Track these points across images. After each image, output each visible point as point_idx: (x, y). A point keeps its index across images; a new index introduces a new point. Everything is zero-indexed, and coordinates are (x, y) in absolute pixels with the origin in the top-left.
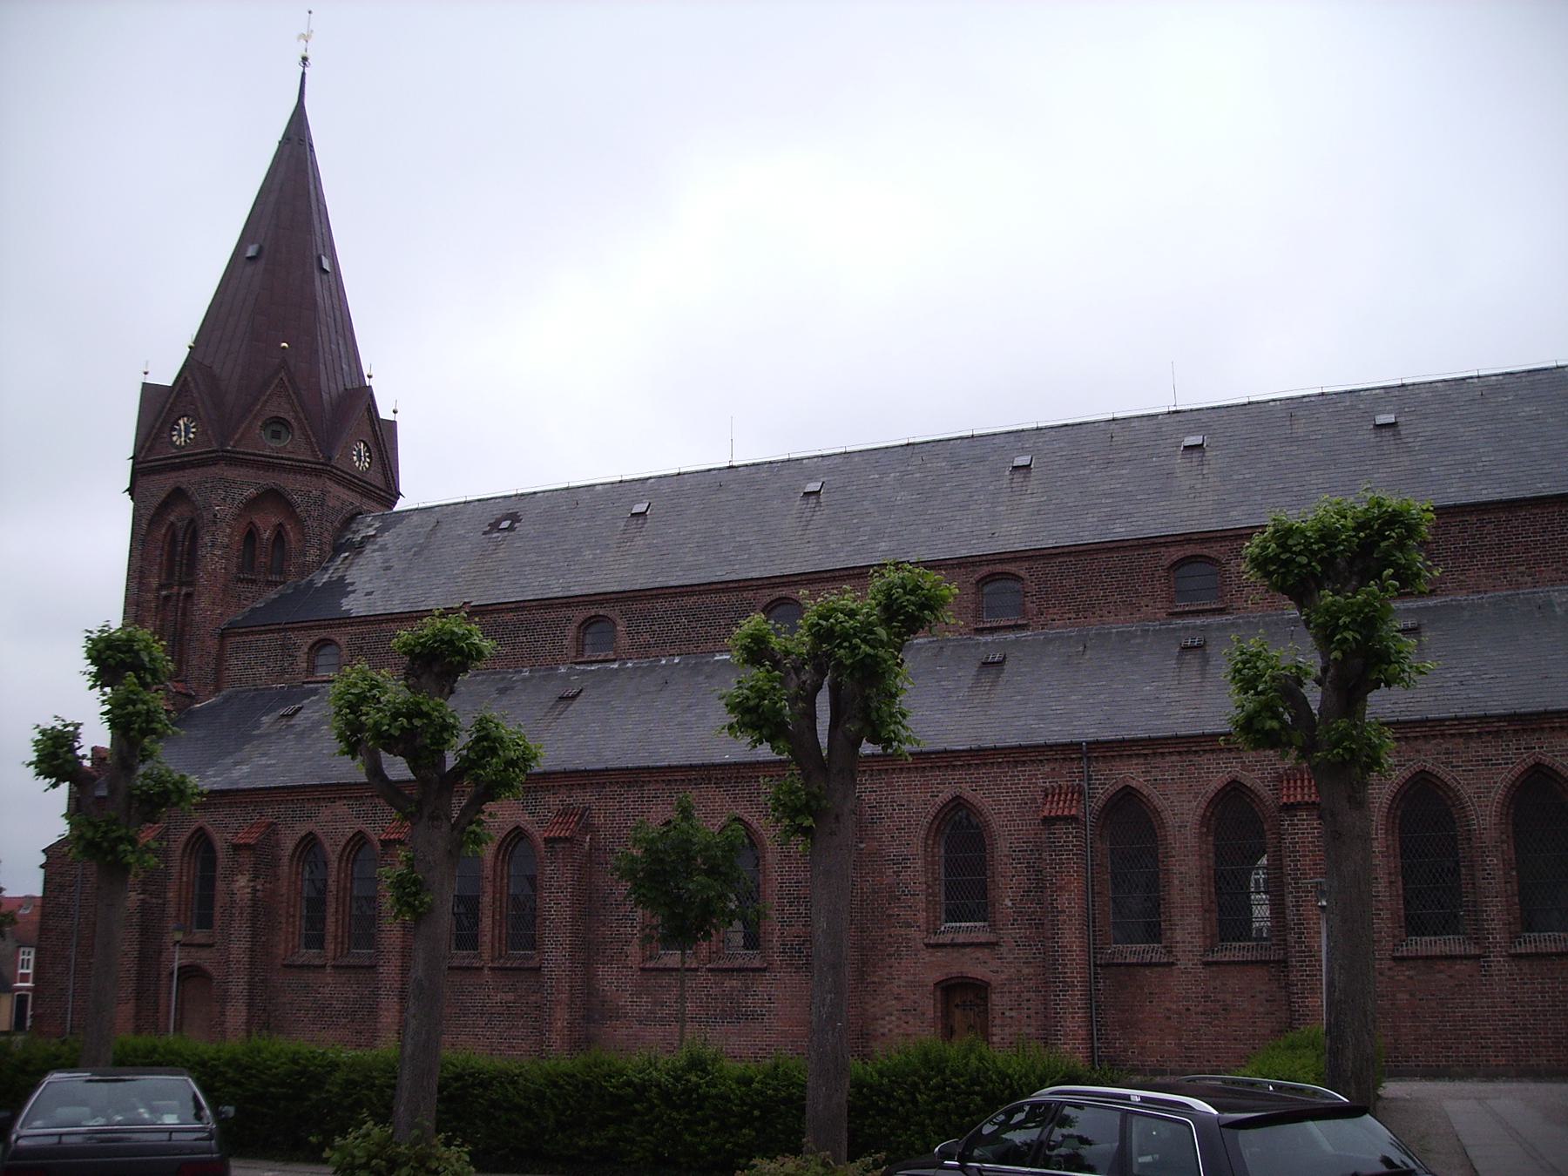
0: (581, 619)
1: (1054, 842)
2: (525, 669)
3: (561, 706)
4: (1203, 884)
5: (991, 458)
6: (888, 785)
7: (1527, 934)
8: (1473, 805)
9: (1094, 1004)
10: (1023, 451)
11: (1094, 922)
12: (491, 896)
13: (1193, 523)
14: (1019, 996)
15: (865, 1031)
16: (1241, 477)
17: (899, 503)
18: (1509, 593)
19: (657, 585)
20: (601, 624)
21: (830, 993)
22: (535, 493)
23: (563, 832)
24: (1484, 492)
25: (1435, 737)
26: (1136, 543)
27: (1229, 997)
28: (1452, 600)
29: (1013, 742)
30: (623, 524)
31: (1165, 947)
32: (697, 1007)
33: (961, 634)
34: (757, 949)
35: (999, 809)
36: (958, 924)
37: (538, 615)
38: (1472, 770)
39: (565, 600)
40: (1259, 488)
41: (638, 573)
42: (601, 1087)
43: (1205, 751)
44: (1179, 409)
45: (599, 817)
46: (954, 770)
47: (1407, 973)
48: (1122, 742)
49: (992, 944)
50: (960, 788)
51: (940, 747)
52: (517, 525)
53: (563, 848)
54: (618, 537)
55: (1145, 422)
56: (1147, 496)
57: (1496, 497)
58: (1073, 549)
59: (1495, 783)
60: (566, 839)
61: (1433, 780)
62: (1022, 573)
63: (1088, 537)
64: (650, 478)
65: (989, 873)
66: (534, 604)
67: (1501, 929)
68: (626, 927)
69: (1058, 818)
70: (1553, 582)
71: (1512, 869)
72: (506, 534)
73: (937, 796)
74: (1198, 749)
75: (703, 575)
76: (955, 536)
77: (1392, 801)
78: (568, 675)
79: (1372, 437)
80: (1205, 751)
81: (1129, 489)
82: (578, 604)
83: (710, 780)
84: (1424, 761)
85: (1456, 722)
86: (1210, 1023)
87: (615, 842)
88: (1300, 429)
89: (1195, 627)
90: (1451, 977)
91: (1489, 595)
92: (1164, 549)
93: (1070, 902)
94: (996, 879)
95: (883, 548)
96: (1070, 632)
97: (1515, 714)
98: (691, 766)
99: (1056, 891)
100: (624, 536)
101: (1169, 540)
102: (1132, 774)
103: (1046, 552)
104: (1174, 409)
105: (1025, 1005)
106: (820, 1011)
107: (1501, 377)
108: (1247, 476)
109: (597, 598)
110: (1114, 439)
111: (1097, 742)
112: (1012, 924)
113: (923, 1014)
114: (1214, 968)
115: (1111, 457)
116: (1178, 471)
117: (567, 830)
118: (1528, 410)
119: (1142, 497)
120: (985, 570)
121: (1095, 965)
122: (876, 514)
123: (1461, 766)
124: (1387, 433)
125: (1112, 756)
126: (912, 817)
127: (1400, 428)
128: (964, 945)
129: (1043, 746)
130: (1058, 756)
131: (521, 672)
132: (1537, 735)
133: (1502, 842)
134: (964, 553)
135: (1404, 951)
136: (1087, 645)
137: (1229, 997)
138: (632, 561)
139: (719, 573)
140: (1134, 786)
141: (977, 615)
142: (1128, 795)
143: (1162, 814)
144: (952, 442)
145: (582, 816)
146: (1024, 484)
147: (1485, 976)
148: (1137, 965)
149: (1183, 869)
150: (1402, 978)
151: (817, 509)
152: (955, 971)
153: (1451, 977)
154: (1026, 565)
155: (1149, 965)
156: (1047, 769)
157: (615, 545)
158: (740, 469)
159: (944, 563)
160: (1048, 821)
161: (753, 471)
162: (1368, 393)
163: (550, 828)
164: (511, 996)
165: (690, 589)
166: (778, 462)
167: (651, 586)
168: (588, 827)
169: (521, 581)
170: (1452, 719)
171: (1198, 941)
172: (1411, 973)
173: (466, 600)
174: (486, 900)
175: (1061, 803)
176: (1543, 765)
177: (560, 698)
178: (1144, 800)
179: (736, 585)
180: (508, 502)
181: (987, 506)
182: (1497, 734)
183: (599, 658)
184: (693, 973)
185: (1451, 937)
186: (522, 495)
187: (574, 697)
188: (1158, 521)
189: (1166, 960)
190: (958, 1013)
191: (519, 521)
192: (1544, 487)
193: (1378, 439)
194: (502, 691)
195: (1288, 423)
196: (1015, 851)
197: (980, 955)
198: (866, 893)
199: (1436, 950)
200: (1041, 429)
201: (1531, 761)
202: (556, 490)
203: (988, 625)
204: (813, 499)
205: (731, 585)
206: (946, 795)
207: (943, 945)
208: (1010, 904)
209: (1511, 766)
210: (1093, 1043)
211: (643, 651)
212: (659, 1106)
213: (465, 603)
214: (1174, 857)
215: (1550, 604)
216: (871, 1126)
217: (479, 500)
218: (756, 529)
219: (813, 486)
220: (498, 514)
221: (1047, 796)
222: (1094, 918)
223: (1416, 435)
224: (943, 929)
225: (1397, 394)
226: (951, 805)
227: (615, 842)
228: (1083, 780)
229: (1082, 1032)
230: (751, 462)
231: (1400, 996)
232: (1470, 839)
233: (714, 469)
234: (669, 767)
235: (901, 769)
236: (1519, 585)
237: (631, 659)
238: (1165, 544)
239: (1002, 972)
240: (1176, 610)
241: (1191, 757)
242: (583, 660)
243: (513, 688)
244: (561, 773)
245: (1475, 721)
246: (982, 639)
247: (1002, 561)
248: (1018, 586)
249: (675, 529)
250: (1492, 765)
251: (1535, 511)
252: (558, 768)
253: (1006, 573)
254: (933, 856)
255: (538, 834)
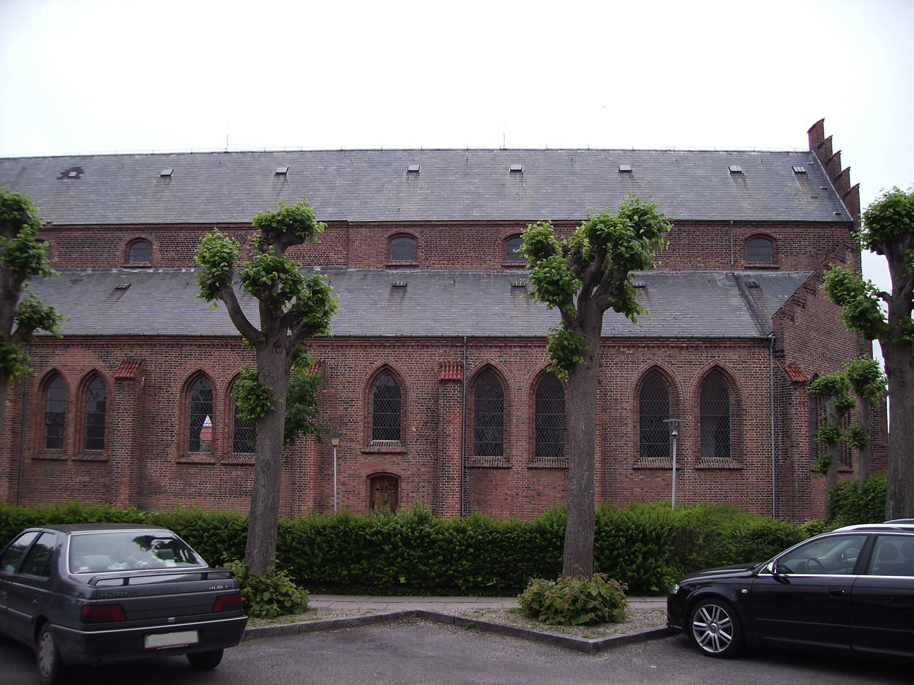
0: (128, 239)
1: (446, 394)
2: (88, 269)
3: (118, 293)
4: (529, 423)
5: (394, 164)
6: (343, 355)
7: (703, 458)
8: (681, 386)
9: (463, 490)
10: (414, 162)
11: (465, 442)
12: (74, 414)
13: (520, 214)
14: (418, 484)
15: (322, 504)
16: (545, 191)
17: (338, 185)
18: (692, 272)
19: (181, 221)
20: (141, 244)
21: (587, 471)
22: (93, 156)
23: (129, 374)
24: (682, 214)
25: (663, 347)
26: (486, 223)
27: (541, 487)
28: (661, 273)
29: (423, 334)
30: (156, 181)
31: (505, 458)
32: (214, 487)
33: (377, 268)
34: (253, 452)
35: (411, 373)
36: (381, 441)
37: (99, 234)
38: (682, 367)
39: (118, 226)
40: (557, 199)
41: (168, 213)
42: (357, 534)
43: (535, 346)
44: (506, 148)
45: (151, 366)
46: (384, 348)
47: (640, 477)
48: (488, 338)
49: (404, 453)
50: (388, 359)
51: (377, 334)
52: (81, 175)
53: (129, 384)
54: (153, 189)
55: (486, 153)
56: (490, 197)
57: (690, 218)
58: (449, 223)
59: (694, 375)
60: (131, 379)
61: (660, 371)
62: (417, 234)
63: (457, 217)
64: (172, 154)
65: (402, 411)
66: (96, 227)
67: (691, 454)
68: (167, 436)
69: (450, 380)
70: (715, 268)
71: (698, 422)
72: (74, 180)
73: (373, 363)
74: (532, 345)
75: (212, 218)
76: (375, 208)
77: (638, 381)
78: (119, 275)
79: (617, 177)
80: (535, 346)
81: (480, 191)
82: (127, 230)
83: (227, 345)
84: (657, 360)
85: (675, 340)
86: (530, 502)
87: (161, 382)
88: (577, 168)
89: (518, 275)
90: (663, 480)
91: (681, 272)
92: (502, 228)
93: (454, 430)
94: (407, 415)
95: (330, 212)
96: (443, 272)
97: (708, 338)
98: (216, 336)
99: (446, 423)
100: (157, 189)
101: (506, 223)
102: (492, 357)
103: (433, 223)
104: (503, 148)
105: (421, 489)
106: (580, 483)
107: (686, 153)
108: (549, 191)
109: (141, 226)
110: (469, 161)
111: (473, 337)
112: (416, 442)
113: (359, 494)
114: (534, 471)
115: (467, 171)
116: (508, 183)
117: (131, 373)
118: (701, 172)
119: (488, 197)
120: (394, 231)
121: (465, 467)
122: (324, 190)
123: (676, 364)
124: (626, 175)
125: (481, 346)
126: (357, 375)
127: (633, 174)
128: (385, 453)
129: (440, 337)
130: (448, 344)
131: (86, 270)
132: (717, 350)
133: (695, 407)
134: (382, 219)
135: (639, 465)
136: (456, 280)
137: (541, 487)
138: (163, 205)
139: (223, 218)
140: (493, 364)
141: (387, 258)
142: (488, 370)
143: (508, 381)
144: (369, 152)
145: (140, 364)
146: (416, 181)
147: (681, 480)
148: (490, 468)
149: (519, 414)
150: (637, 479)
151: (285, 184)
152: (379, 469)
153: (663, 480)
154: (419, 229)
155: (498, 468)
156: (441, 351)
157: (151, 194)
158: (232, 154)
159: (369, 223)
160: (443, 382)
161: (241, 156)
162: (614, 152)
163: (119, 371)
164: (87, 479)
165: (204, 226)
166: (257, 153)
167: (177, 222)
168: (144, 372)
169: (86, 212)
170: (674, 338)
171: (525, 456)
172: (642, 477)
173: (49, 221)
174: (71, 416)
175: (451, 372)
176: (719, 366)
177: (116, 289)
178: (498, 373)
179: (234, 226)
180: (73, 160)
181: (393, 192)
182: (697, 348)
183: (140, 265)
184: (212, 466)
185: (663, 458)
186: (84, 156)
187: (126, 289)
188: (499, 212)
189: (506, 466)
190: (378, 494)
191: (82, 173)
192: (714, 215)
193: (622, 179)
194: (75, 282)
195: (570, 164)
196: (419, 399)
197: (395, 459)
198: (326, 420)
199: (656, 465)
200: (424, 150)
201: (713, 364)
202: (108, 155)
203: (395, 264)
204: (282, 177)
205: (231, 226)
206: (378, 363)
207: (374, 453)
208: (415, 430)
209: (702, 366)
210: (461, 513)
211: (171, 263)
212: (401, 547)
213: (48, 223)
214: (514, 406)
215: (714, 280)
216: (550, 558)
217: (53, 157)
218: (246, 192)
219: (283, 170)
220: (67, 166)
221: (441, 367)
222: (465, 440)
223: (643, 179)
224: (372, 443)
225: (630, 154)
226: (381, 369)
227: (161, 382)
228: (463, 359)
229: (458, 506)
230: (240, 150)
231: (636, 489)
232: (678, 405)
233: (215, 153)
234: (201, 336)
235: (351, 346)
236: (697, 268)
237: (162, 267)
238: (502, 225)
239: (409, 470)
240: (507, 264)
241: (527, 349)
242: (129, 265)
243: (81, 280)
244: (127, 336)
245: (686, 340)
246: (390, 272)
247: (405, 226)
248: (413, 242)
249: (192, 188)
250: (693, 365)
251: (708, 228)
252: (125, 333)
253: (407, 234)
254: (369, 399)
255: (109, 375)
